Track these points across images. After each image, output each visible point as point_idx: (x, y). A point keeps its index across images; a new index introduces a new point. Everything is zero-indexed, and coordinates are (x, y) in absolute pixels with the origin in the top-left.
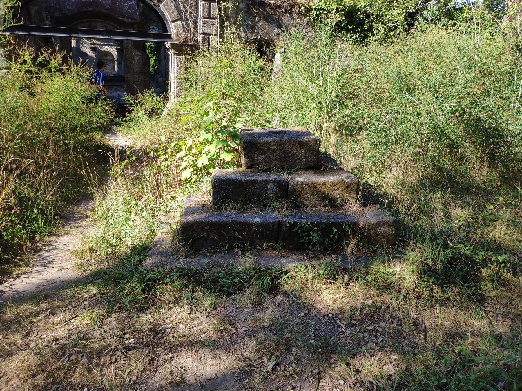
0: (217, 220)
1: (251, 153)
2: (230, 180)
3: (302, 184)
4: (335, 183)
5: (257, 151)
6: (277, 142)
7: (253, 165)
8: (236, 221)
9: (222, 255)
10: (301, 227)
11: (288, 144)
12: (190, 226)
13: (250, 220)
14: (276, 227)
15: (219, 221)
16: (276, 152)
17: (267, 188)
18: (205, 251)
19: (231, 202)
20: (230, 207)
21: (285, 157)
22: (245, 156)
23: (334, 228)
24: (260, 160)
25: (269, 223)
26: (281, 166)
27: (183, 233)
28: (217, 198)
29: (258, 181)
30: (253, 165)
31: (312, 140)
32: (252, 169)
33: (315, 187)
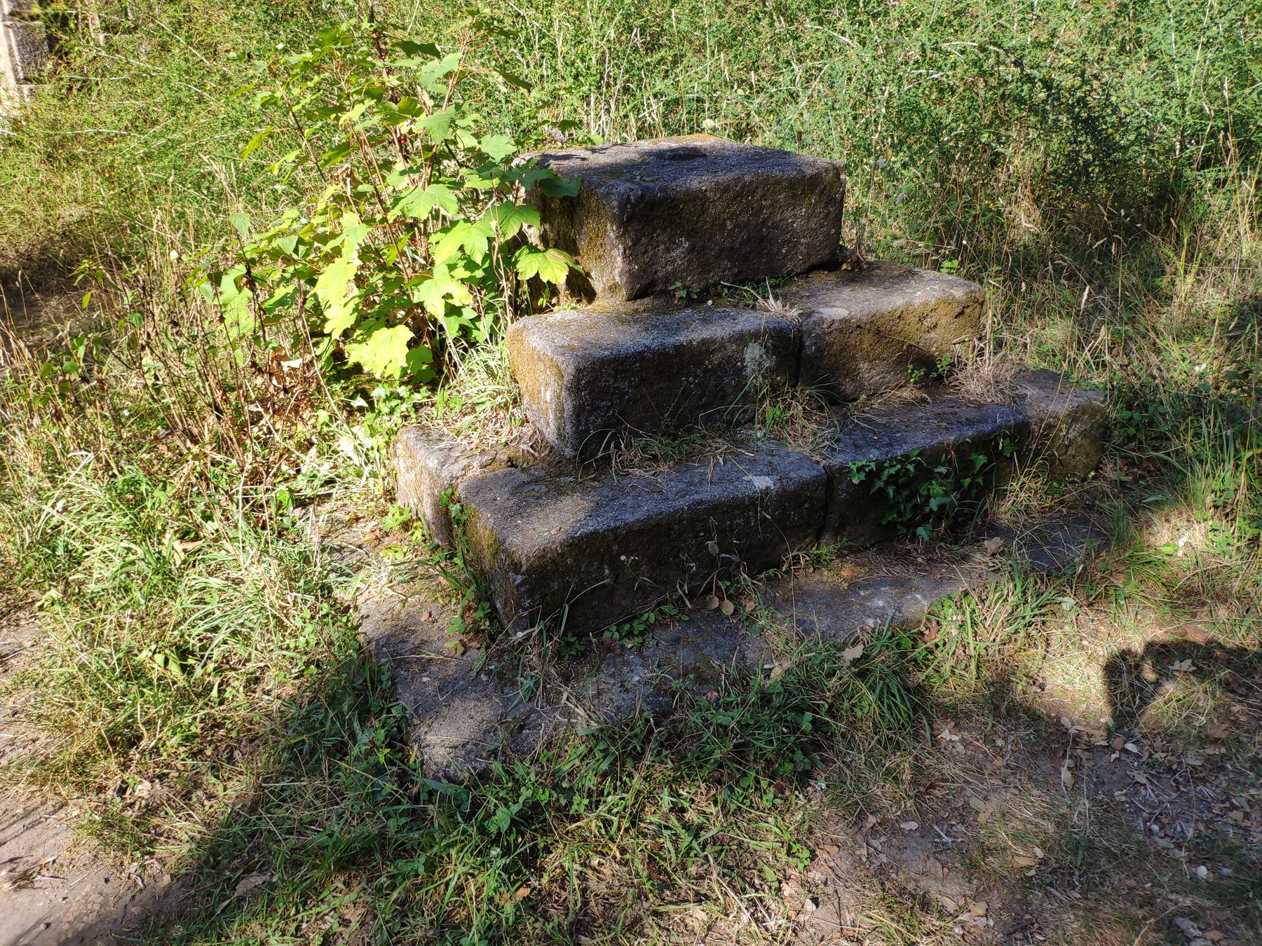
0: (640, 514)
1: (644, 240)
2: (627, 357)
3: (846, 326)
4: (929, 308)
5: (664, 229)
6: (726, 190)
7: (652, 284)
8: (701, 502)
9: (674, 630)
10: (893, 479)
11: (760, 192)
12: (554, 561)
13: (741, 490)
14: (821, 492)
15: (650, 518)
16: (722, 227)
17: (743, 360)
18: (611, 634)
19: (637, 435)
20: (635, 455)
21: (749, 239)
22: (625, 256)
23: (974, 456)
24: (674, 261)
25: (803, 486)
26: (738, 274)
27: (531, 593)
28: (587, 431)
29: (714, 341)
30: (652, 284)
31: (827, 170)
32: (646, 300)
33: (878, 332)
